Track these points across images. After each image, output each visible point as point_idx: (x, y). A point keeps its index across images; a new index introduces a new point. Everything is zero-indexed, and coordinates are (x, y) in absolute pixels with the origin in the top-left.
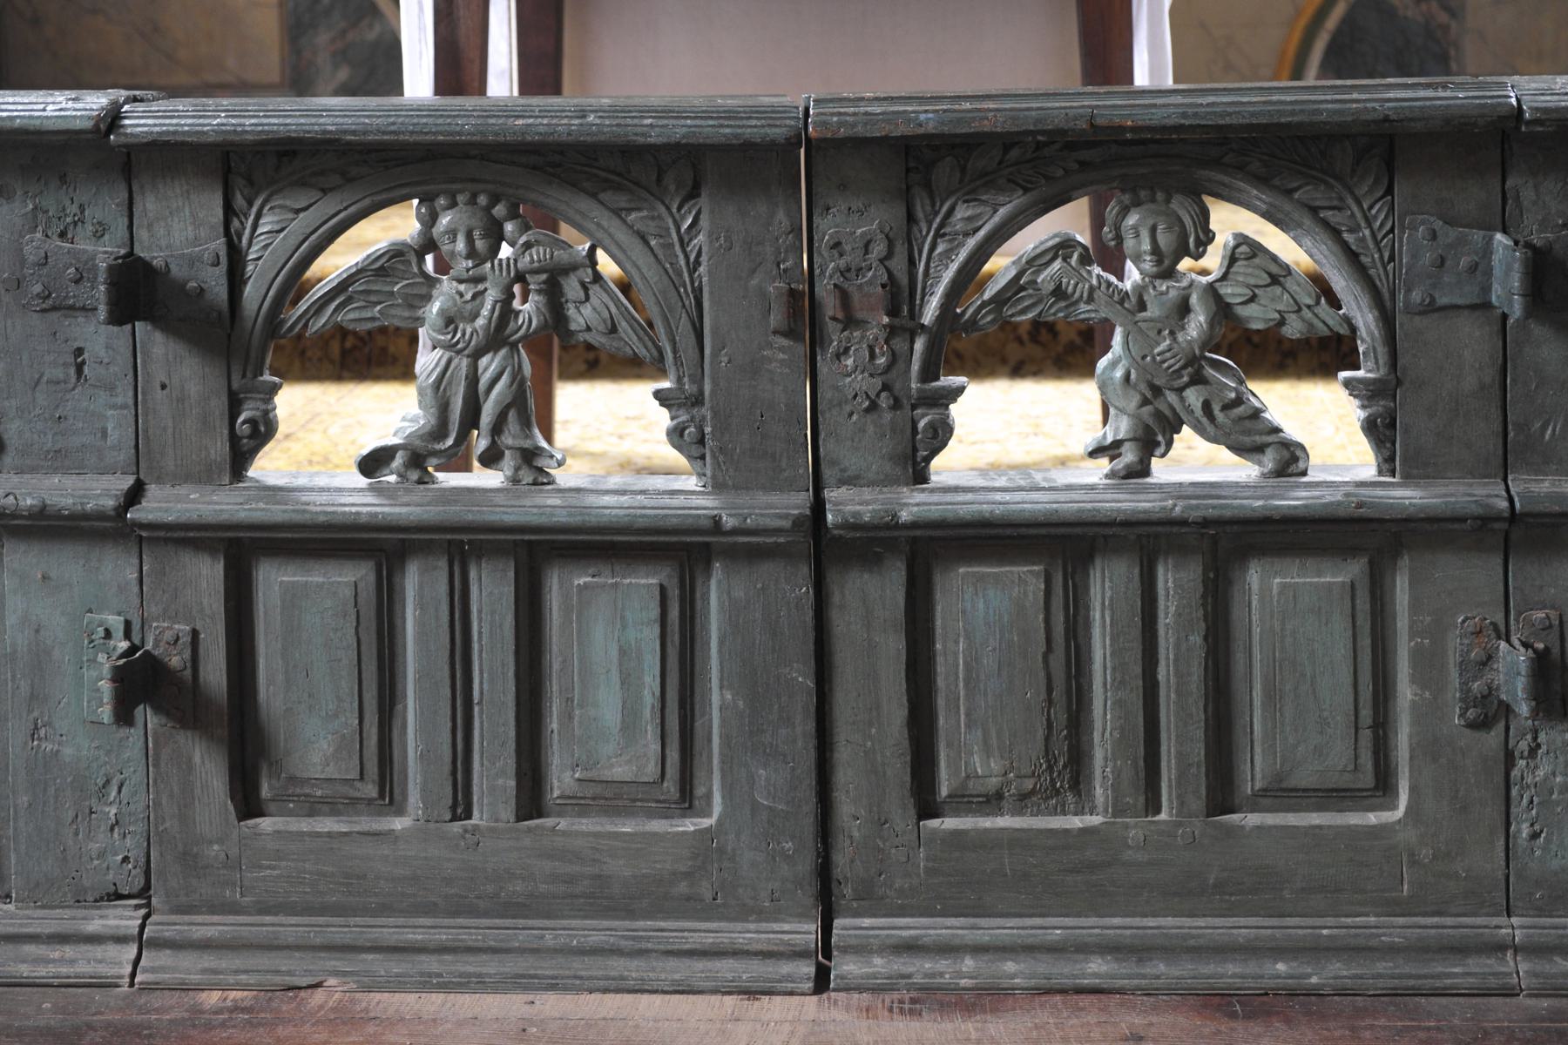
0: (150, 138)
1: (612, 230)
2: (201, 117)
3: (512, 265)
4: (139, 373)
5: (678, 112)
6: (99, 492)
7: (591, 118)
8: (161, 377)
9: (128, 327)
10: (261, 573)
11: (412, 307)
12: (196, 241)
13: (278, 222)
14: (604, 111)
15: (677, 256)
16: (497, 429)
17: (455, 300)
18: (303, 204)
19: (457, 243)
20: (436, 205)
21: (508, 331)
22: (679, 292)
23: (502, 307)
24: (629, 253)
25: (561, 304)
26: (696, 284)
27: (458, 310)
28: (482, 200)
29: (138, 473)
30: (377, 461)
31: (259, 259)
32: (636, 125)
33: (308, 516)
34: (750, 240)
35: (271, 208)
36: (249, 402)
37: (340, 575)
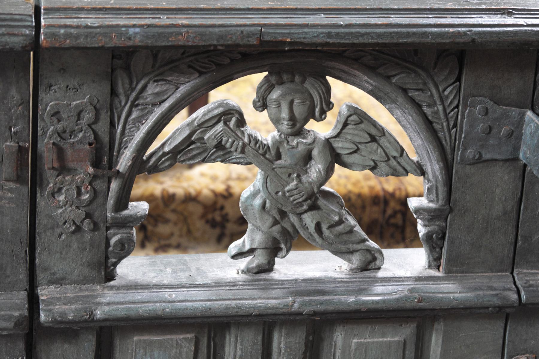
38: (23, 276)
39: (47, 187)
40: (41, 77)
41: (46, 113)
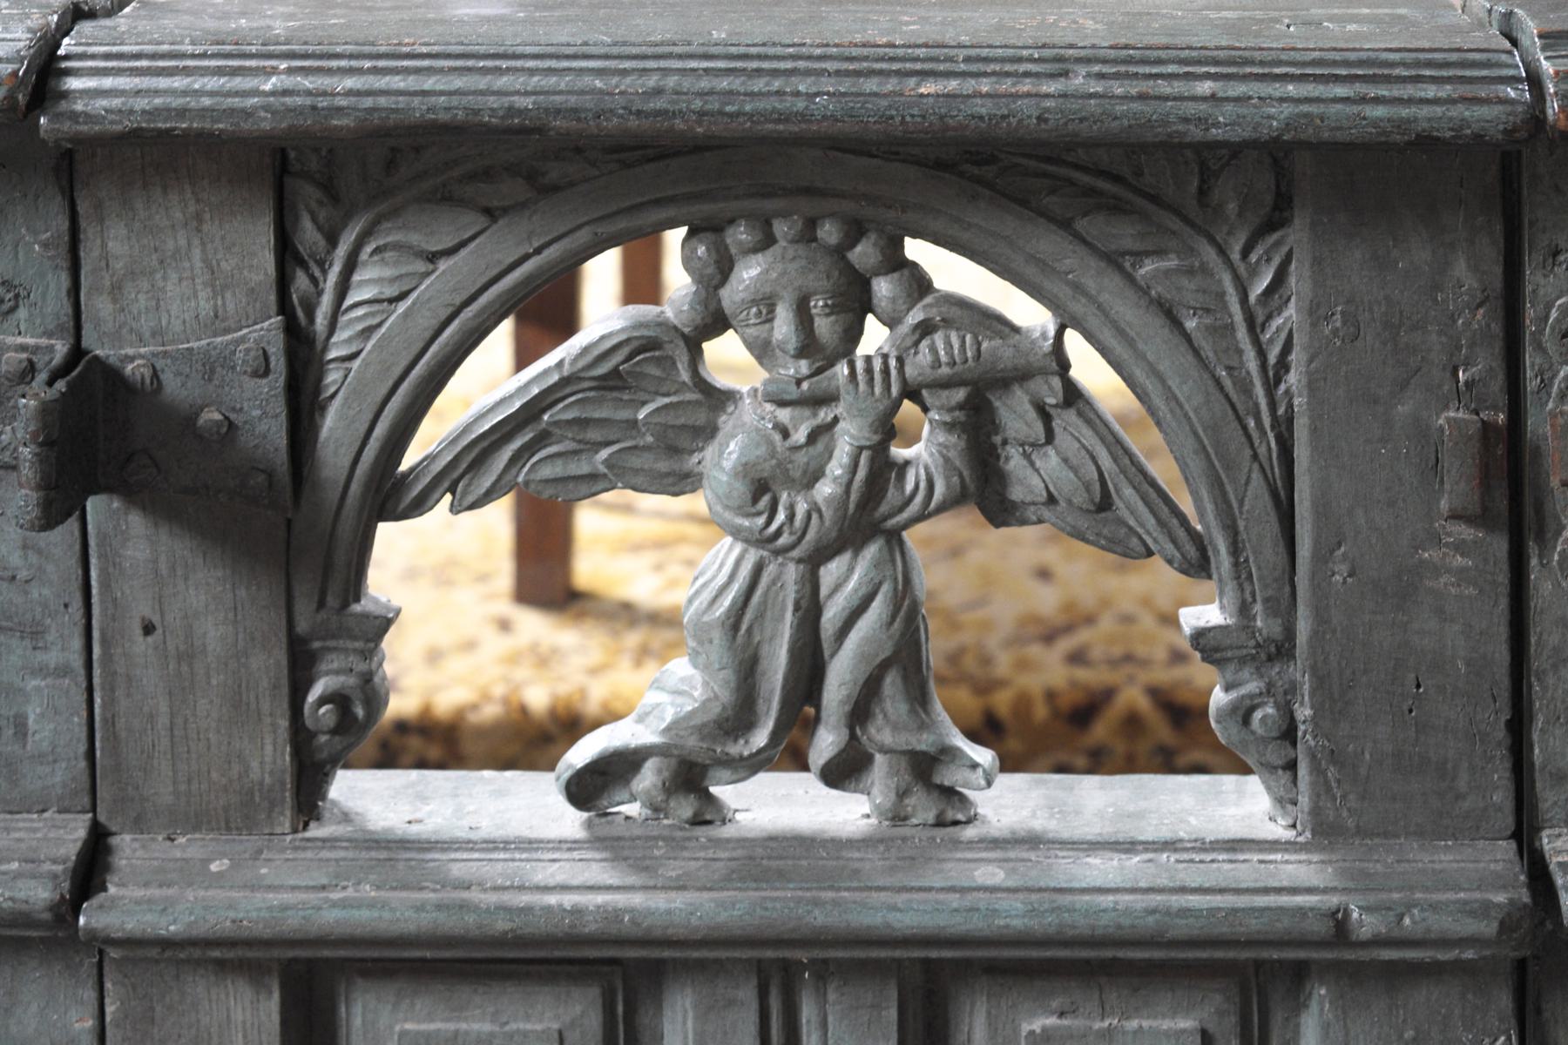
0: (128, 124)
1: (1105, 297)
2: (234, 72)
3: (894, 372)
4: (95, 599)
5: (1262, 63)
6: (15, 865)
7: (1078, 82)
8: (143, 608)
9: (72, 524)
10: (357, 1009)
11: (674, 451)
12: (217, 322)
13: (393, 280)
14: (1105, 61)
15: (1240, 352)
16: (860, 711)
17: (770, 443)
18: (448, 242)
19: (777, 323)
20: (729, 241)
21: (884, 508)
22: (1245, 428)
23: (872, 460)
24: (1141, 346)
25: (993, 447)
26: (1281, 411)
27: (779, 464)
28: (829, 232)
29: (94, 809)
30: (603, 773)
31: (352, 357)
32: (1180, 98)
33: (470, 919)
34: (1395, 321)
35: (377, 251)
36: (330, 657)
37: (528, 1018)
38: (1502, 797)
39: (1557, 540)
40: (1530, 228)
41: (1548, 329)
